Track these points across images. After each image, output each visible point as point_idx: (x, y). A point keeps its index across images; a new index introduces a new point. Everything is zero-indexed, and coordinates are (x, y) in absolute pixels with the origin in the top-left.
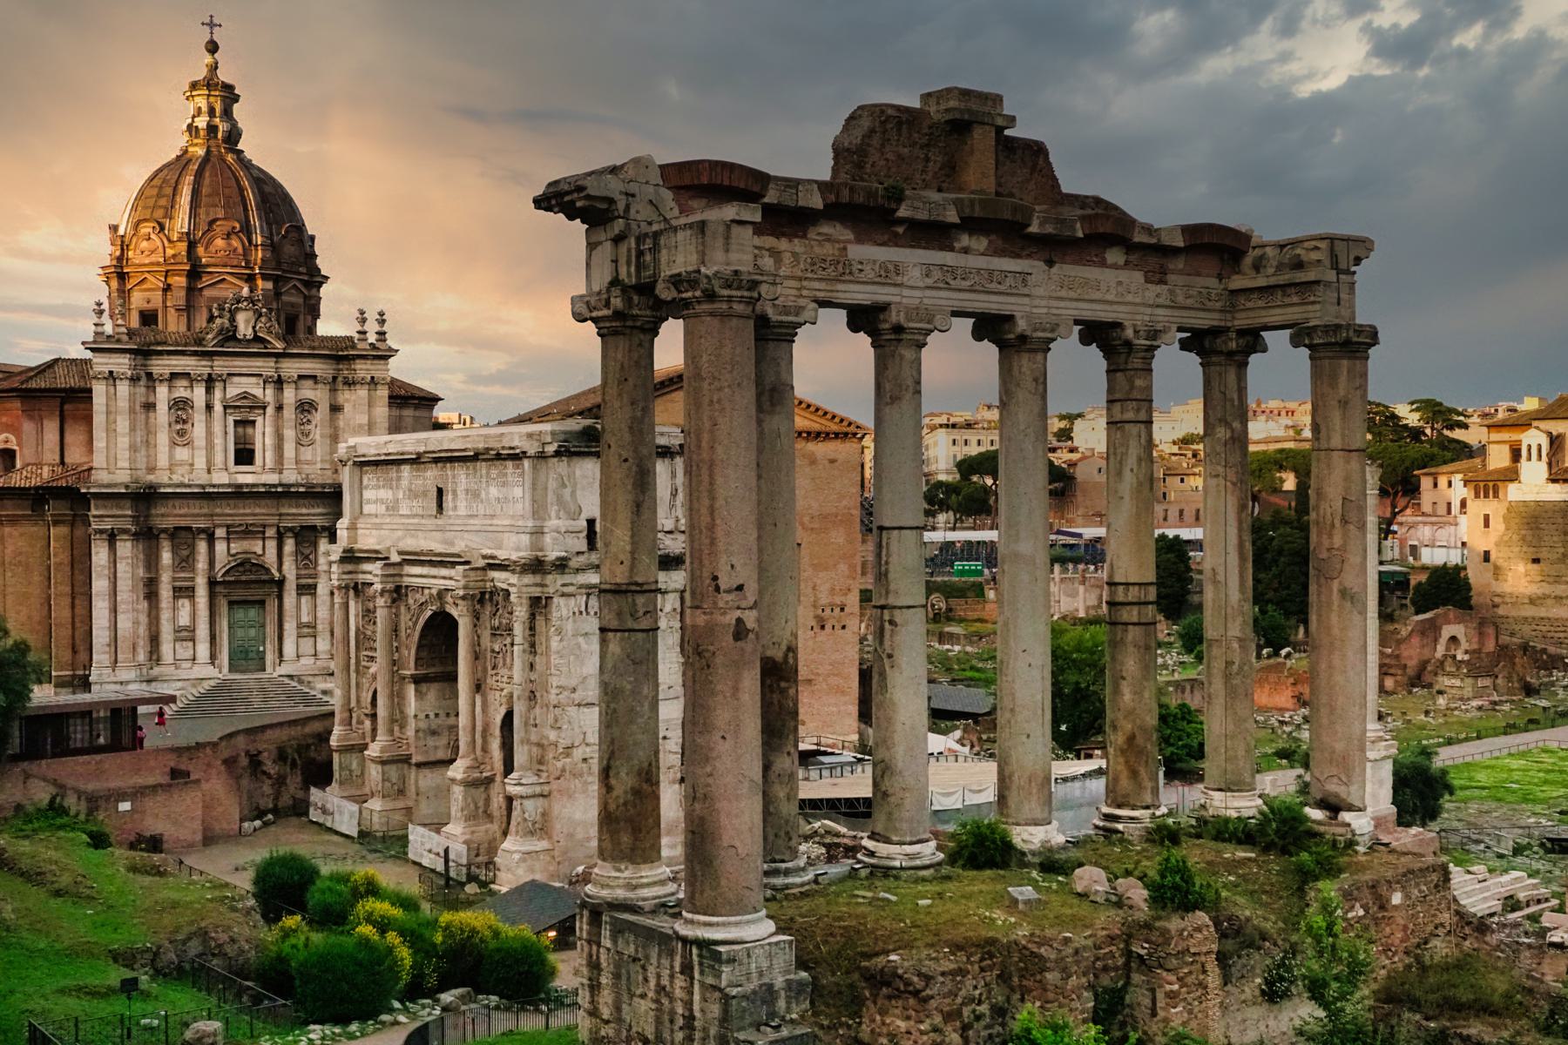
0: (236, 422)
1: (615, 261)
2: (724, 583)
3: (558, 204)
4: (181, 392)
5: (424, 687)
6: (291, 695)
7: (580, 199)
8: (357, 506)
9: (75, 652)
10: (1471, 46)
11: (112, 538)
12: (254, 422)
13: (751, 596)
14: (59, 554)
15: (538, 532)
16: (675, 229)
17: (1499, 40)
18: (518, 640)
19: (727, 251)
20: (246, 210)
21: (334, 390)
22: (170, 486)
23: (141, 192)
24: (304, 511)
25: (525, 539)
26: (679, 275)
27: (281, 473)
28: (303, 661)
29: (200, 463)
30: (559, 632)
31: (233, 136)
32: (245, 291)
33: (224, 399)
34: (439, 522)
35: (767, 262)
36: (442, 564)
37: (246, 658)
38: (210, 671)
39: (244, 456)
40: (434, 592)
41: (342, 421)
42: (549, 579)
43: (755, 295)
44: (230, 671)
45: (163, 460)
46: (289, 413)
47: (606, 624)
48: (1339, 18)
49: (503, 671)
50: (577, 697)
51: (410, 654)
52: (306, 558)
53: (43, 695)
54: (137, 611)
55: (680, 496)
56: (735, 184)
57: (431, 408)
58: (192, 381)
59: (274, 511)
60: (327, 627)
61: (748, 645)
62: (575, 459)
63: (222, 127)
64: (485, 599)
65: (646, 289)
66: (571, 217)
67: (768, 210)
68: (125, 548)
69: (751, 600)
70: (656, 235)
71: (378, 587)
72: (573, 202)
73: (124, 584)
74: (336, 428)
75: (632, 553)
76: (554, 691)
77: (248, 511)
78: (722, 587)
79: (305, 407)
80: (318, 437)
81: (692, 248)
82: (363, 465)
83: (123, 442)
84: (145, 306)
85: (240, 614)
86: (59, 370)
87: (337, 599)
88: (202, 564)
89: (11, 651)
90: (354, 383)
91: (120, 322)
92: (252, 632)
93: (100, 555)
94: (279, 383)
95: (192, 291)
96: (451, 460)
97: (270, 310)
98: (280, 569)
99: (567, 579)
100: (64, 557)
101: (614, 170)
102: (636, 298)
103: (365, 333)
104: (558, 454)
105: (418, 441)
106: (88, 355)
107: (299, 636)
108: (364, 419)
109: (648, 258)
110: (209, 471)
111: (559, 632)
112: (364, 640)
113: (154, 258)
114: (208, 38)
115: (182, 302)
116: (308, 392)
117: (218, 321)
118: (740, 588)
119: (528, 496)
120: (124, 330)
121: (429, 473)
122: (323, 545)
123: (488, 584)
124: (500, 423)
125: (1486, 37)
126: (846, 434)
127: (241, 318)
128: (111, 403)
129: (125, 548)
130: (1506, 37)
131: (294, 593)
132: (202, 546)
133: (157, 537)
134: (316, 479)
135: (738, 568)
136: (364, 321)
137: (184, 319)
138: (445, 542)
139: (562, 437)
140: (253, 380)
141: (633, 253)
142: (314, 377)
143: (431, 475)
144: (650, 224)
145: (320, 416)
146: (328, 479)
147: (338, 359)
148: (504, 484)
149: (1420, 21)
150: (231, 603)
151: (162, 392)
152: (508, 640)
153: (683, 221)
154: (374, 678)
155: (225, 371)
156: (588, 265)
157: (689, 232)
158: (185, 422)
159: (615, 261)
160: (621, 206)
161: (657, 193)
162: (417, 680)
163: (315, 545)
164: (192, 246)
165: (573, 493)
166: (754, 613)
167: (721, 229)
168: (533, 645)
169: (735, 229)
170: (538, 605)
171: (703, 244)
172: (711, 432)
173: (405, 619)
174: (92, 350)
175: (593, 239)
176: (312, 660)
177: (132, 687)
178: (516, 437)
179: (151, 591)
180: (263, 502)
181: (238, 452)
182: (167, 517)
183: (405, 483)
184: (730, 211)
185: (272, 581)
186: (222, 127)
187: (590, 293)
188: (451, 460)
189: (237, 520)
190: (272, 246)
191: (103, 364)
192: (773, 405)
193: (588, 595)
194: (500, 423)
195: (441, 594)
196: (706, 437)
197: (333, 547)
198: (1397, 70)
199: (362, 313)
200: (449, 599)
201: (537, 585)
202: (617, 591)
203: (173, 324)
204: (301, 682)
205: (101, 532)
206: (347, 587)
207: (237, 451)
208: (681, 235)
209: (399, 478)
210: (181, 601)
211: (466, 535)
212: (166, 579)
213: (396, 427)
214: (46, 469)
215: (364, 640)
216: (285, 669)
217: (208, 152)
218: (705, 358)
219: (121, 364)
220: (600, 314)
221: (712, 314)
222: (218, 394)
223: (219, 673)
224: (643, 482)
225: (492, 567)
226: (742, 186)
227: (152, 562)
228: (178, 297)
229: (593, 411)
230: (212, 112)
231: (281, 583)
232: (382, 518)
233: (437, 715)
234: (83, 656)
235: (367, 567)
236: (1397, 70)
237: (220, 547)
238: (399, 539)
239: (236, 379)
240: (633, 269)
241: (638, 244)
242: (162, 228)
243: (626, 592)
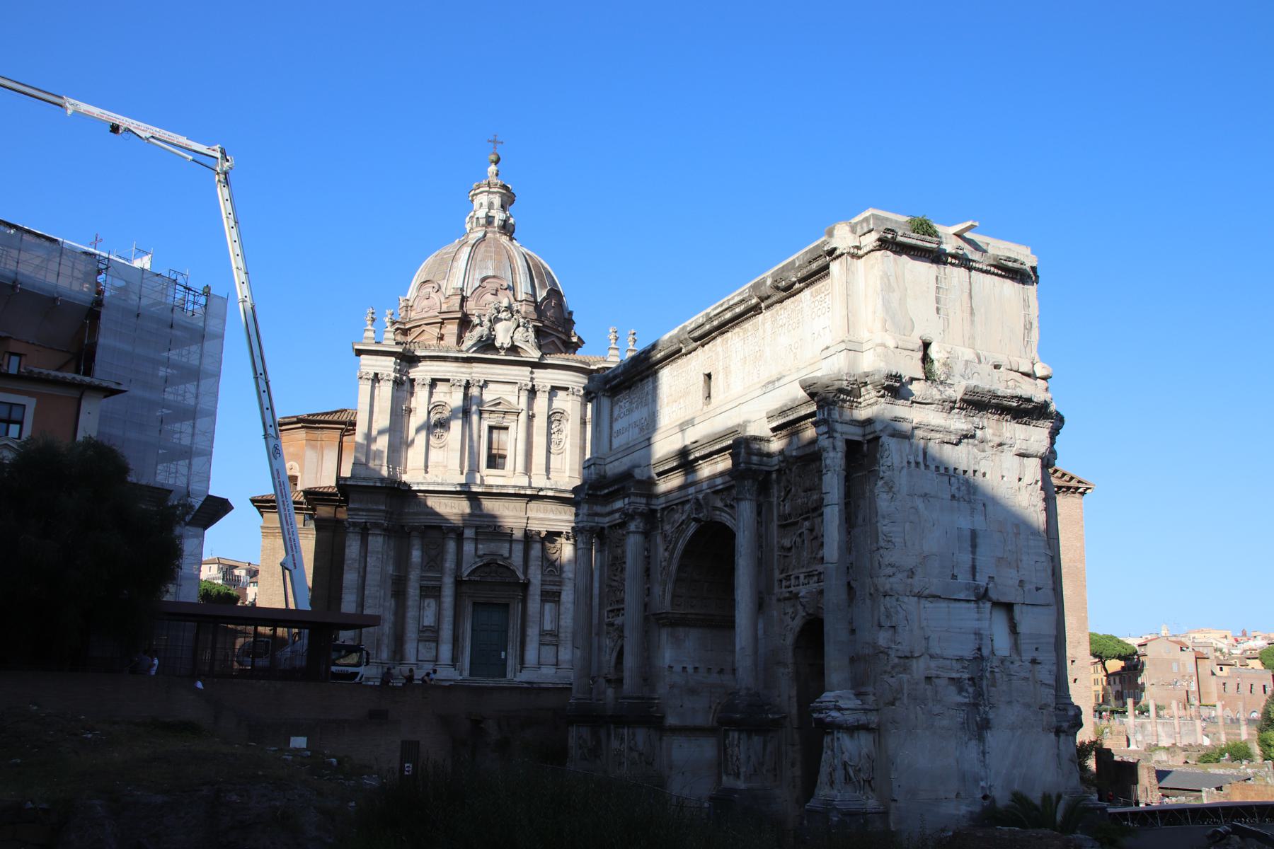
11: (364, 531)
24: (551, 516)
30: (890, 488)
37: (488, 656)
50: (917, 582)
55: (1035, 334)
73: (373, 578)
88: (449, 564)
93: (353, 548)
107: (541, 644)
126: (1069, 488)
129: (376, 542)
131: (538, 598)
132: (451, 546)
150: (475, 604)
173: (661, 552)
176: (552, 670)
179: (399, 591)
212: (414, 576)
216: (524, 677)
227: (402, 562)
231: (526, 586)
233: (696, 668)
237: (468, 547)
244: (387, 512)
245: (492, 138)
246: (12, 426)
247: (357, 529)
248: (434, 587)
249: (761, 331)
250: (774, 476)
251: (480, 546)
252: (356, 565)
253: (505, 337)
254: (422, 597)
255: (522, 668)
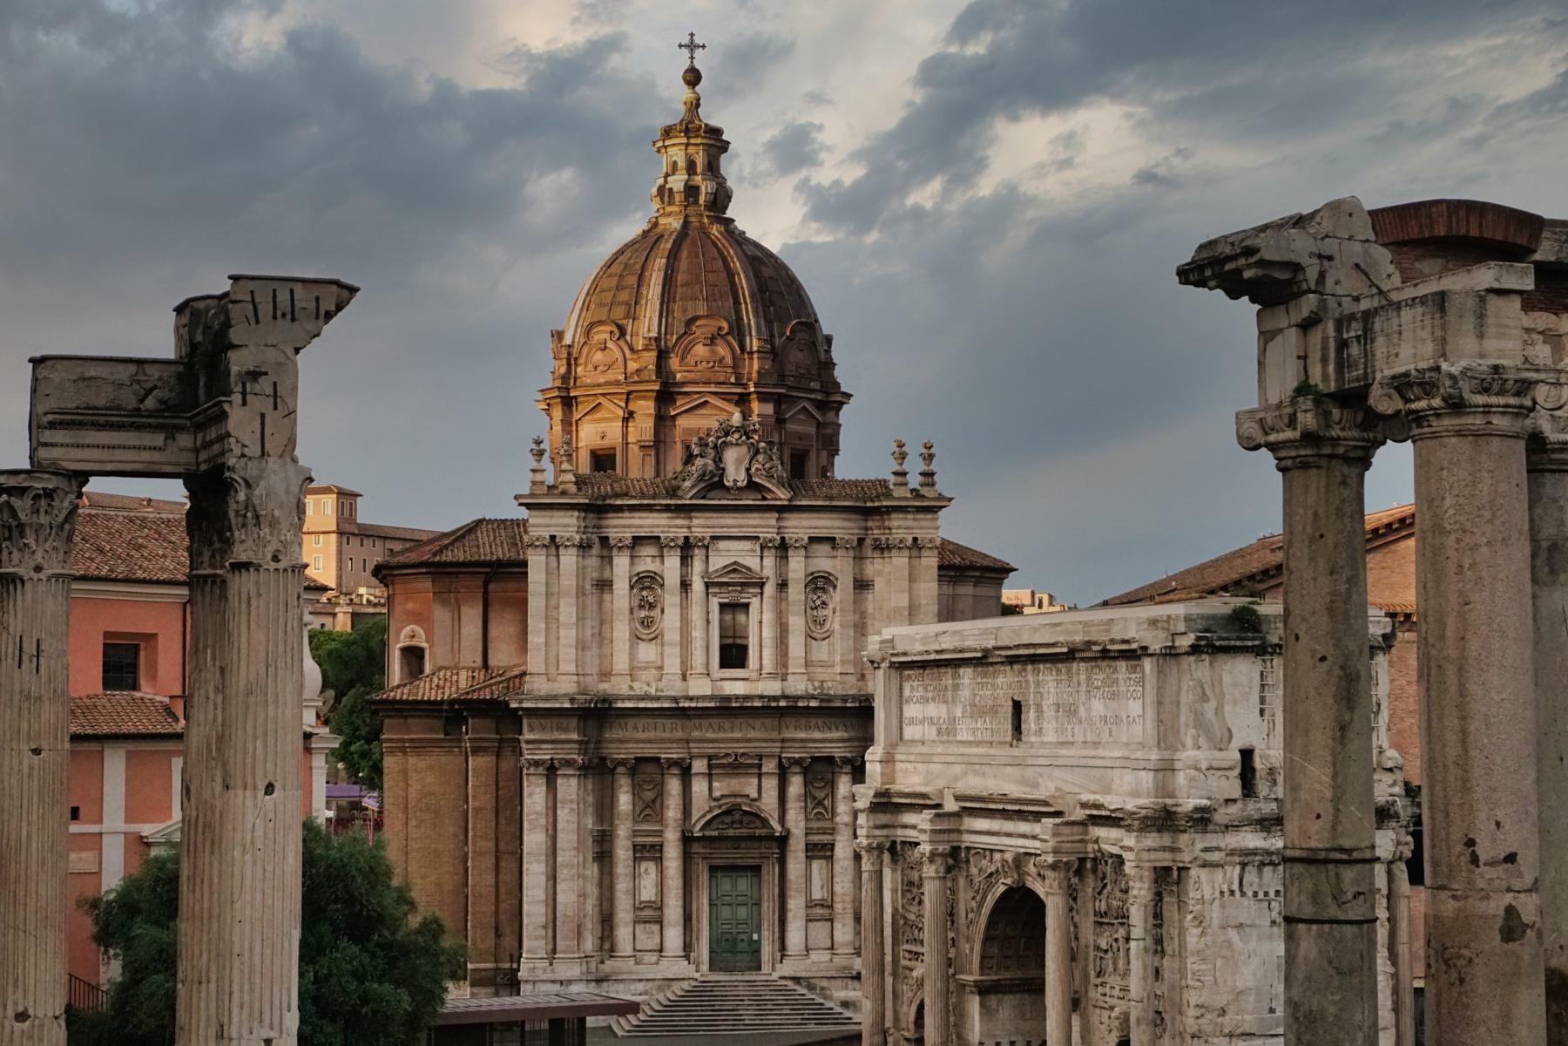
0: (722, 606)
1: (1303, 358)
2: (1484, 853)
3: (1214, 276)
4: (647, 564)
5: (993, 1000)
6: (799, 1006)
7: (1249, 266)
8: (895, 730)
9: (498, 935)
10: (928, 205)
11: (551, 772)
12: (747, 606)
13: (1528, 870)
14: (479, 796)
15: (1166, 769)
16: (1398, 306)
17: (961, 198)
18: (1137, 932)
19: (1481, 336)
20: (737, 303)
21: (859, 559)
22: (629, 698)
23: (595, 284)
24: (817, 735)
25: (1147, 779)
26: (1406, 375)
27: (784, 679)
28: (814, 956)
29: (673, 665)
30: (1200, 920)
31: (721, 199)
32: (736, 418)
33: (706, 573)
34: (1015, 752)
35: (1542, 353)
36: (1021, 815)
37: (735, 950)
38: (683, 968)
39: (734, 655)
40: (1009, 857)
41: (871, 601)
42: (1184, 839)
43: (1528, 403)
44: (713, 967)
45: (621, 662)
46: (796, 592)
47: (1293, 911)
48: (769, 175)
49: (1113, 980)
50: (1228, 1022)
51: (972, 950)
52: (819, 804)
53: (459, 997)
54: (584, 877)
56: (1488, 235)
57: (999, 583)
58: (662, 548)
59: (774, 735)
60: (849, 906)
61: (1526, 949)
62: (1222, 658)
63: (706, 187)
64: (1086, 869)
65: (1353, 398)
66: (1234, 294)
67: (1544, 272)
68: (568, 786)
69: (1528, 881)
70: (1368, 316)
71: (926, 848)
72: (1238, 272)
73: (567, 839)
74: (863, 615)
75: (1336, 800)
76: (1192, 1012)
77: (738, 735)
78: (1483, 856)
79: (819, 583)
80: (837, 626)
81: (1426, 334)
82: (903, 667)
83: (568, 635)
84: (598, 443)
85: (726, 884)
86: (482, 536)
87: (866, 865)
88: (673, 812)
89: (418, 932)
90: (888, 548)
91: (565, 466)
92: (742, 912)
93: (535, 796)
94: (783, 548)
95: (663, 421)
96: (1034, 659)
97: (770, 444)
98: (782, 820)
99: (1213, 840)
100: (487, 800)
101: (1299, 221)
102: (1336, 413)
103: (904, 474)
104: (1195, 650)
105: (985, 632)
106: (523, 513)
107: (809, 920)
108: (903, 600)
109: (1355, 350)
110: (684, 678)
111: (1200, 920)
112: (905, 928)
113: (610, 376)
114: (687, 65)
115: (649, 436)
116: (824, 561)
117: (699, 462)
118: (1511, 858)
119: (1151, 713)
120: (570, 477)
121: (1000, 680)
122: (844, 785)
123: (1090, 847)
124: (1105, 604)
125: (946, 194)
127: (730, 456)
128: (552, 580)
129: (568, 786)
130: (970, 194)
131: (802, 855)
132: (674, 786)
133: (612, 772)
134: (834, 688)
135: (1507, 825)
136: (903, 456)
137: (651, 461)
138: (1024, 782)
139: (1201, 625)
140: (747, 545)
141: (1332, 345)
142: (831, 540)
143: (1005, 683)
144: (1357, 299)
145: (840, 596)
146: (851, 687)
147: (866, 513)
148: (1114, 696)
149: (867, 176)
150: (713, 869)
151: (621, 563)
152: (1121, 932)
153: (1409, 293)
154: (920, 984)
155: (708, 533)
156: (1261, 364)
157: (1419, 310)
158: (652, 606)
159: (1303, 358)
160: (1312, 274)
161: (1366, 253)
162: (984, 990)
163: (832, 785)
164: (662, 356)
165: (1219, 711)
166: (1534, 899)
167: (1471, 303)
168: (1159, 941)
169: (1494, 303)
170: (1167, 879)
171: (1444, 327)
172: (1462, 616)
173: (964, 899)
174: (529, 506)
175: (1269, 326)
176: (826, 956)
177: (575, 988)
178: (1132, 625)
179: (603, 854)
180: (758, 723)
181: (724, 649)
182: (626, 743)
183: (965, 694)
184: (1485, 276)
185: (771, 838)
186: (706, 187)
187: (1267, 408)
188: (1034, 659)
189: (723, 749)
190: (773, 353)
191: (542, 525)
192: (1552, 572)
193: (1244, 865)
194: (1105, 604)
195: (1020, 860)
196: (1451, 623)
197: (858, 788)
198: (840, 236)
199: (901, 446)
200: (1032, 869)
201: (1164, 849)
202: (1311, 860)
203: (637, 468)
204: (811, 988)
205: (537, 763)
206: (880, 848)
207: (723, 648)
208: (1407, 315)
209: (956, 687)
210: (644, 865)
211: (1057, 772)
212: (623, 831)
213: (948, 613)
214: (463, 674)
215: (905, 928)
216: (788, 968)
217: (686, 224)
218: (1448, 501)
219: (567, 525)
220: (1281, 436)
221: (1459, 433)
222: (697, 566)
223: (696, 971)
224: (1350, 690)
225: (1095, 820)
226: (1499, 237)
227: (605, 809)
228: (644, 425)
229: (1264, 579)
230: (691, 167)
231: (783, 840)
232: (931, 747)
234: (508, 942)
235: (909, 818)
236: (840, 236)
237: (699, 787)
238: (956, 778)
239: (722, 545)
240: (1331, 368)
241: (1339, 330)
242: (623, 333)
243: (1327, 861)
244: (581, 742)
245: (686, 41)
246: (174, 760)
247: (541, 770)
248: (653, 846)
249: (1075, 679)
250: (1089, 865)
251: (716, 784)
252: (543, 821)
253: (737, 470)
254: (636, 860)
255: (783, 956)
